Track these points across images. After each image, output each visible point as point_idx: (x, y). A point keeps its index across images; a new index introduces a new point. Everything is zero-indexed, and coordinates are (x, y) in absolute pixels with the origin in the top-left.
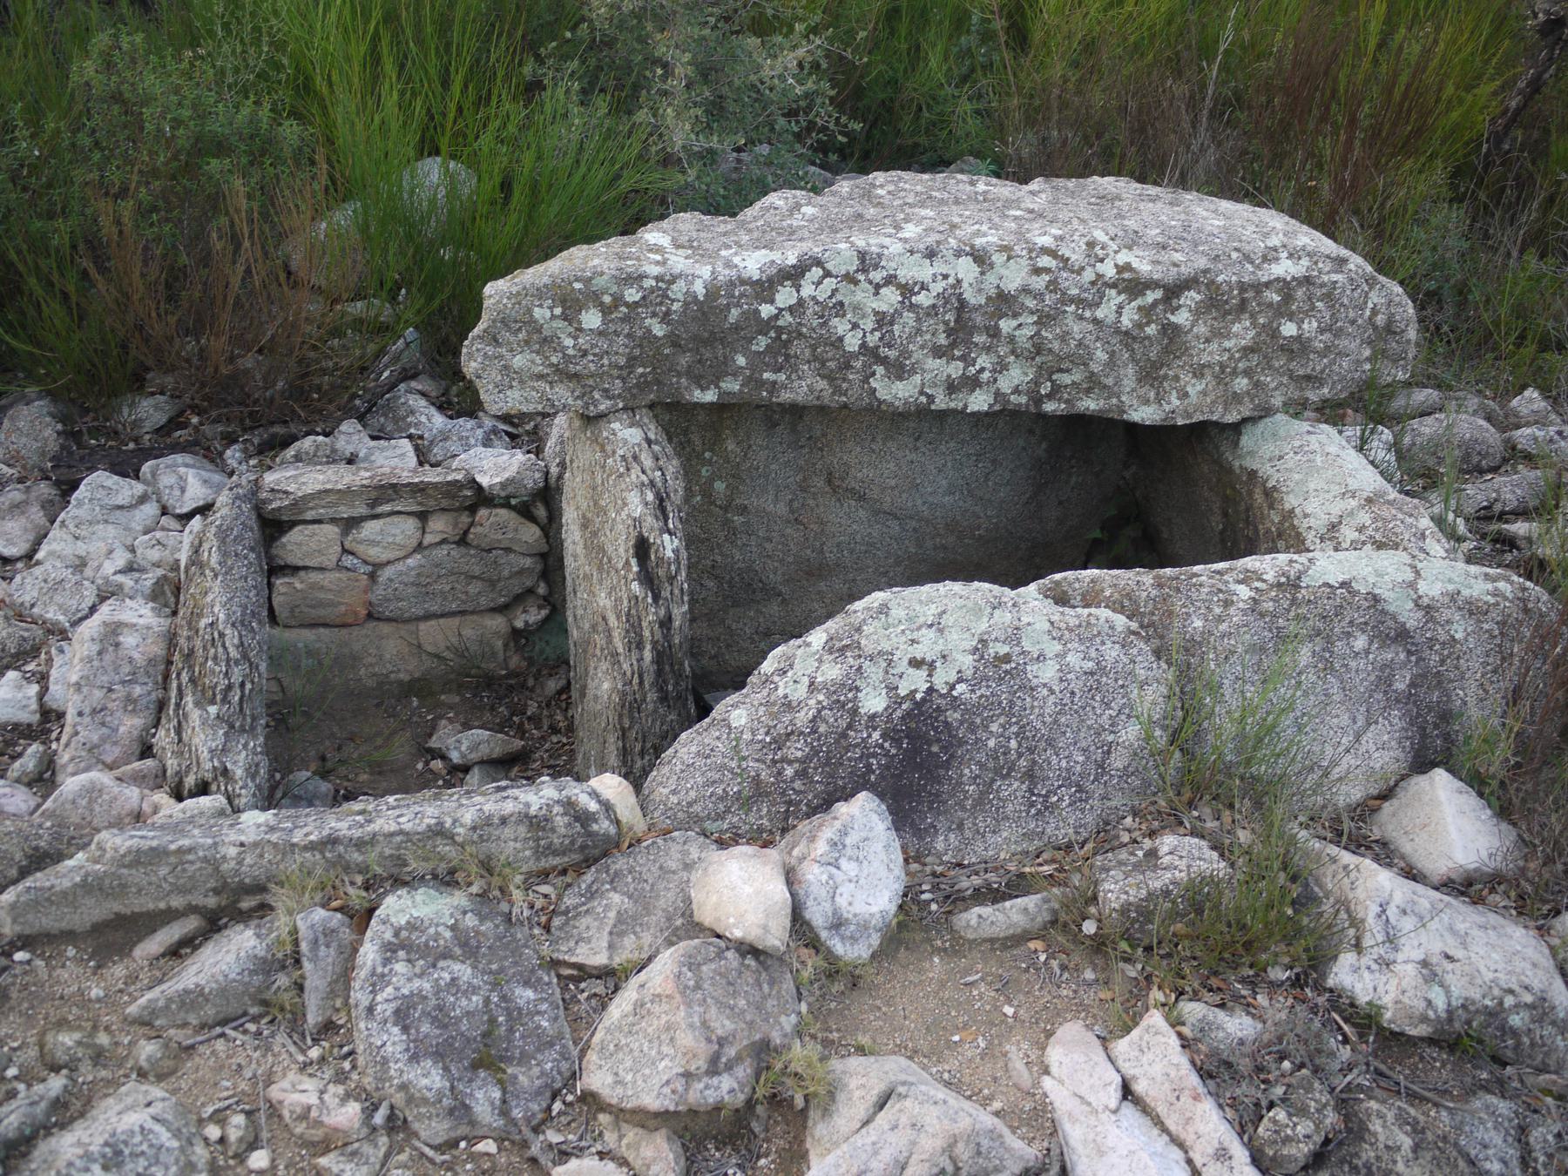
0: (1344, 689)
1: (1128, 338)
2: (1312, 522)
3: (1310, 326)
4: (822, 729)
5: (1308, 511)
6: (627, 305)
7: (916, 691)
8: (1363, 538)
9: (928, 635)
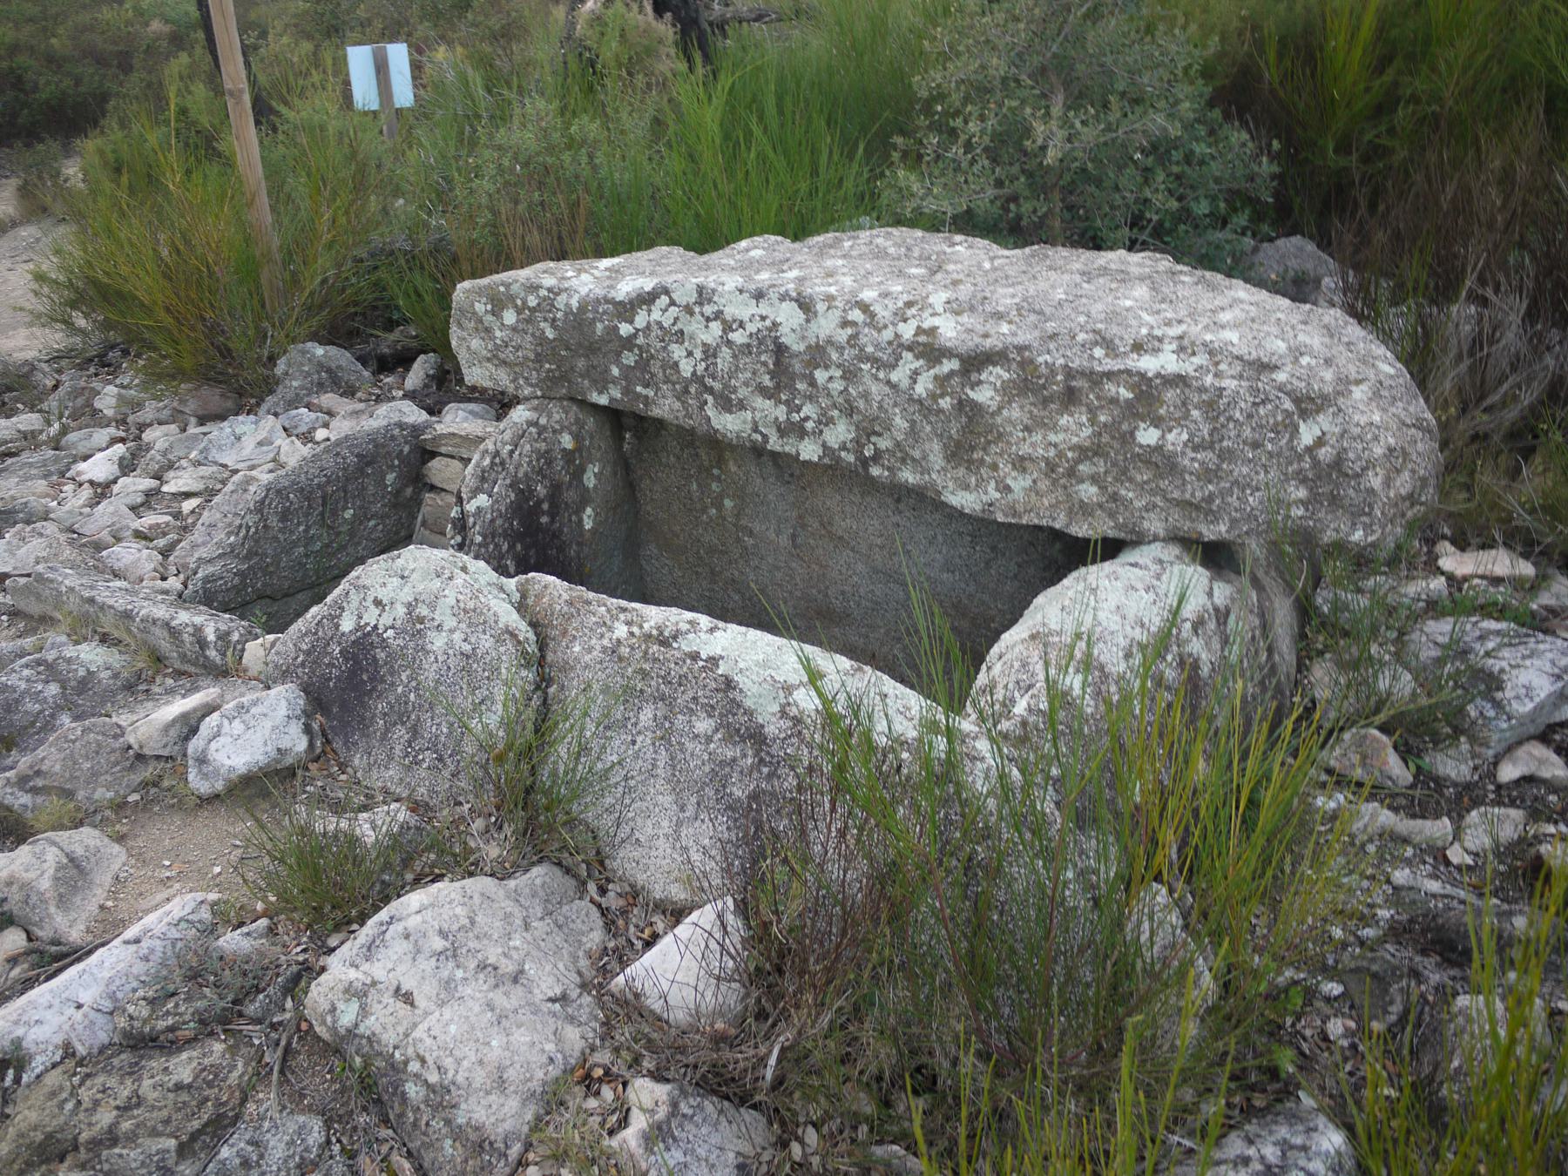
0: (674, 767)
1: (926, 407)
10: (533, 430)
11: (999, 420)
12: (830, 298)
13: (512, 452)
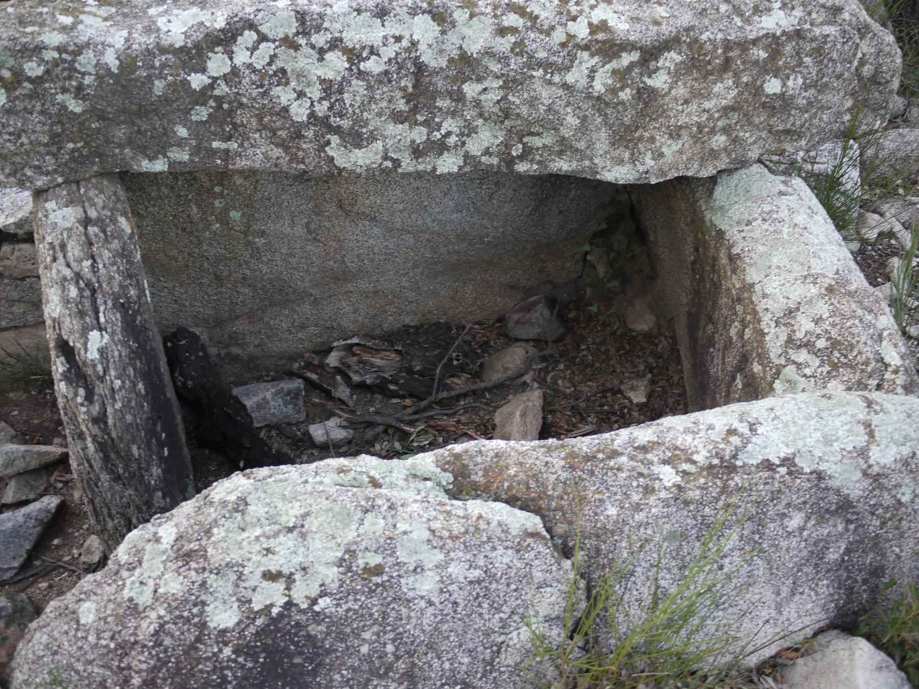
2: (770, 304)
3: (795, 83)
4: (168, 641)
5: (767, 291)
6: (30, 80)
7: (272, 605)
8: (818, 331)
9: (288, 541)
10: (93, 230)
11: (667, 99)
13: (94, 268)
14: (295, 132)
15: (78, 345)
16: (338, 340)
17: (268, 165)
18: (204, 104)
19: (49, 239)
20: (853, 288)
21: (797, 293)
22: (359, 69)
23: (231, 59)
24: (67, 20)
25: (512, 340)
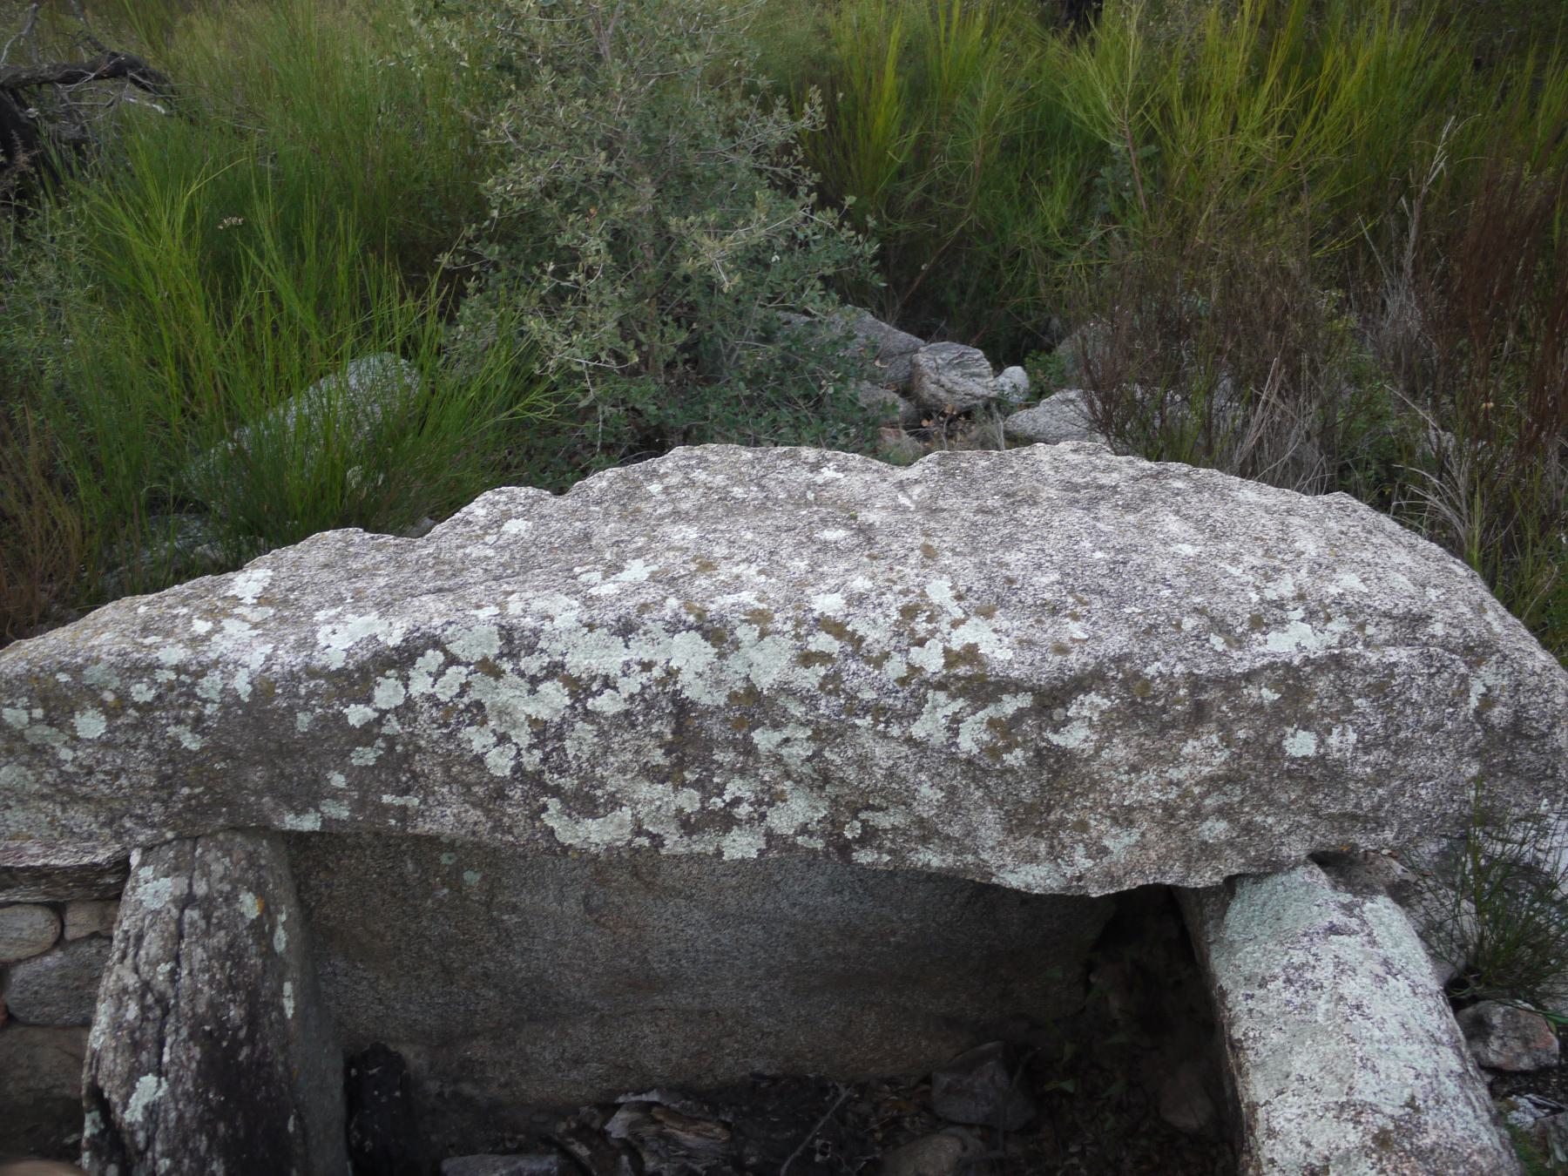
6: (136, 706)
10: (192, 914)
11: (1095, 766)
12: (759, 618)
13: (173, 976)
14: (495, 790)
15: (115, 1098)
16: (626, 1092)
17: (463, 832)
18: (369, 744)
19: (126, 925)
20: (1427, 1141)
21: (1324, 1138)
22: (585, 708)
23: (406, 687)
24: (201, 627)
25: (939, 1124)
